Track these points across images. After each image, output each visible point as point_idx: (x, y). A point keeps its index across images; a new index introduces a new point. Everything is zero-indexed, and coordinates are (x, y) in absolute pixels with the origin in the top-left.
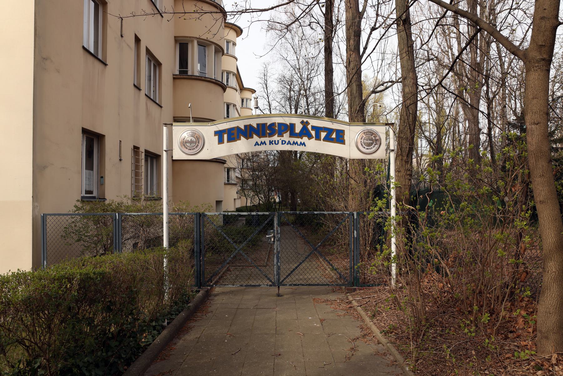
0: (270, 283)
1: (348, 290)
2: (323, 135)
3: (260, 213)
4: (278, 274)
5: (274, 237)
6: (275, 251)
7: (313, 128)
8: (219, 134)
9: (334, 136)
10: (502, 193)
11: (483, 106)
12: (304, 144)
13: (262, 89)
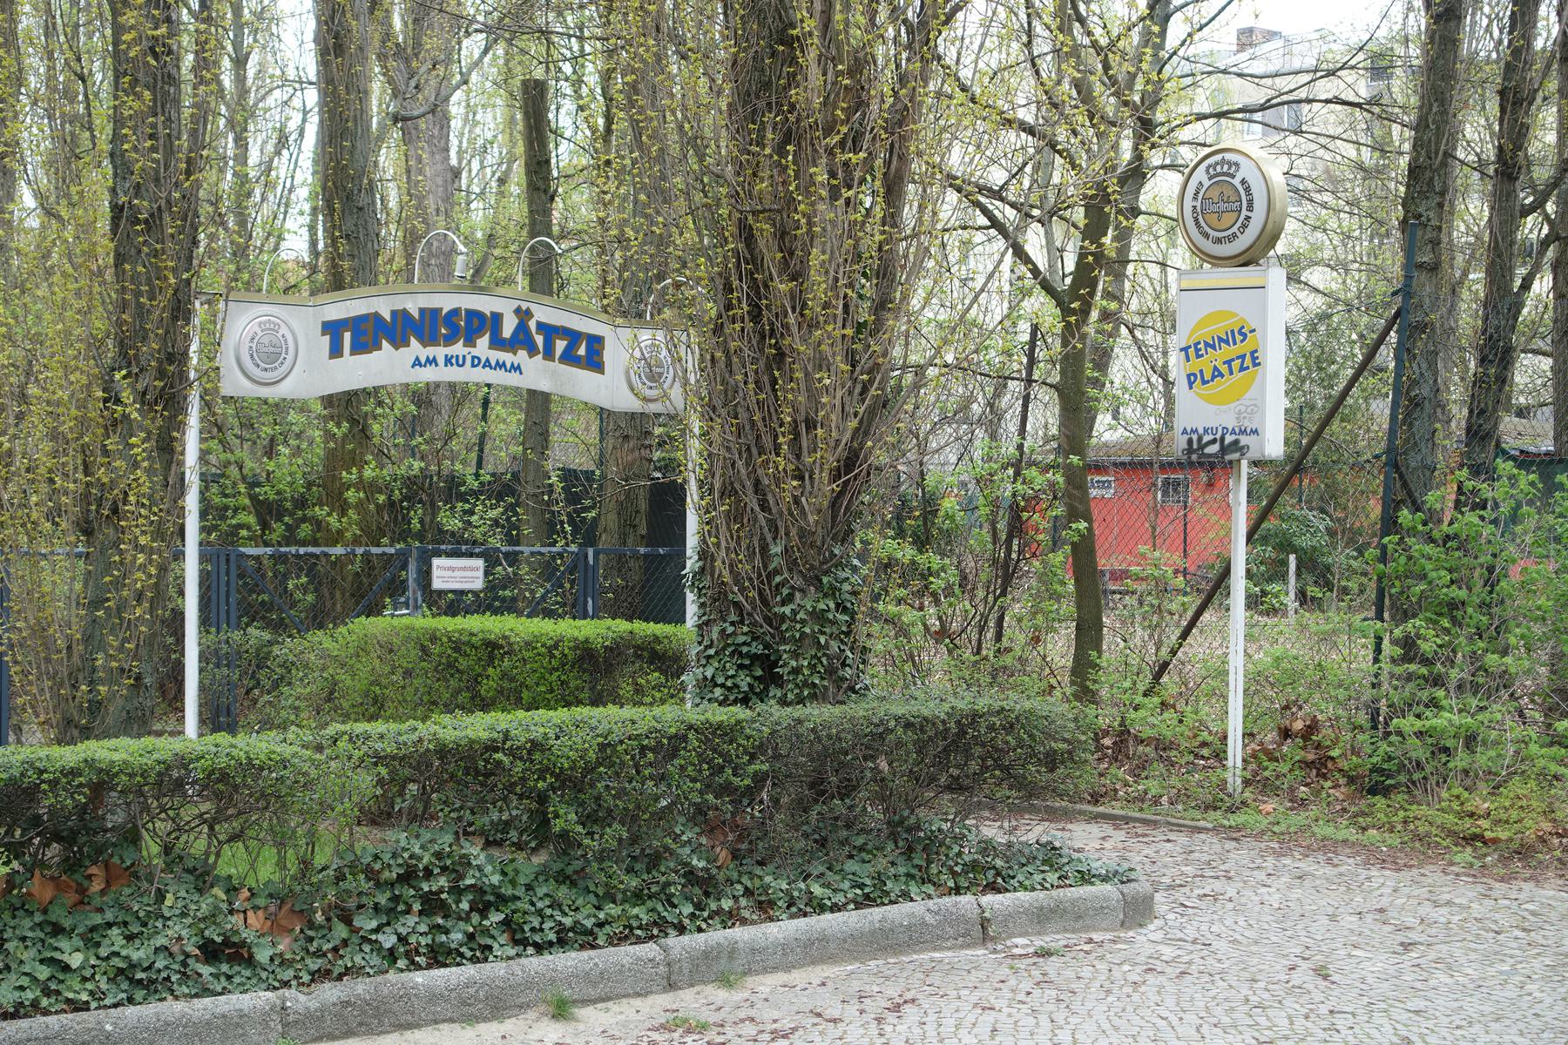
2: (560, 345)
7: (541, 326)
9: (582, 351)
12: (517, 368)
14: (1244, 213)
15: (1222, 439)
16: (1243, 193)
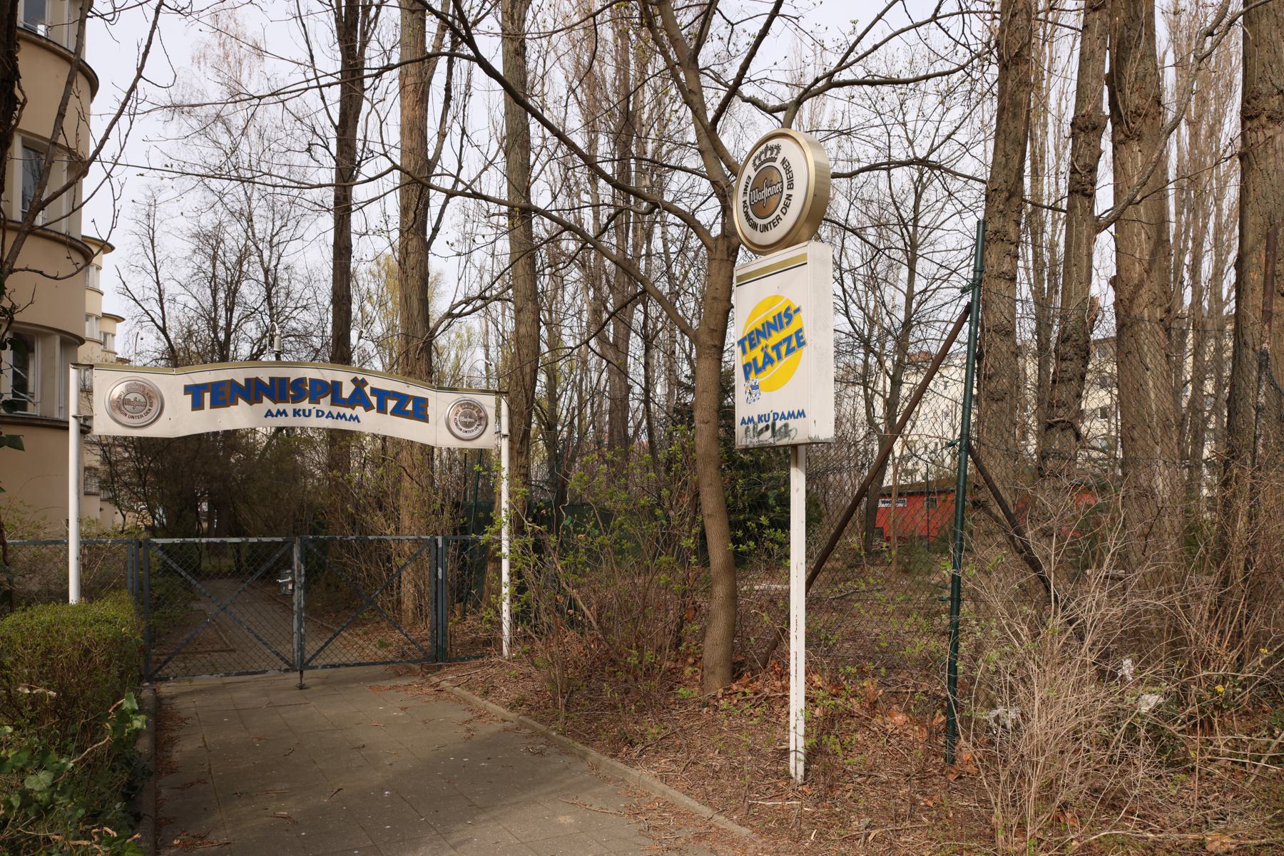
0: (286, 666)
1: (428, 668)
2: (391, 404)
3: (264, 539)
4: (301, 648)
5: (293, 582)
6: (295, 608)
7: (374, 391)
8: (195, 392)
9: (410, 407)
10: (667, 505)
11: (636, 344)
12: (356, 419)
13: (141, 249)
14: (786, 192)
15: (774, 425)
16: (783, 172)
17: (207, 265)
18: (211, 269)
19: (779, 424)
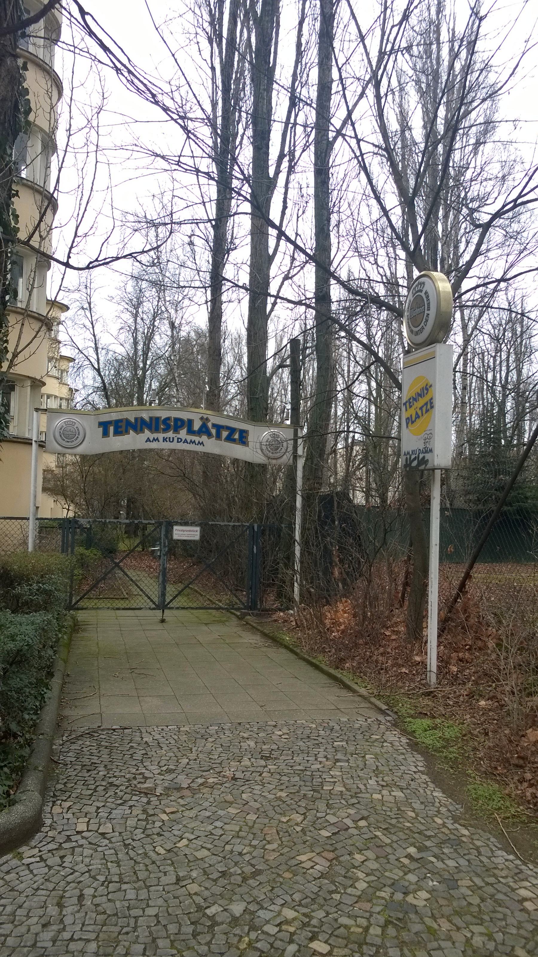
2: (225, 434)
7: (214, 425)
9: (237, 436)
14: (426, 312)
17: (131, 321)
18: (133, 324)
19: (421, 456)
